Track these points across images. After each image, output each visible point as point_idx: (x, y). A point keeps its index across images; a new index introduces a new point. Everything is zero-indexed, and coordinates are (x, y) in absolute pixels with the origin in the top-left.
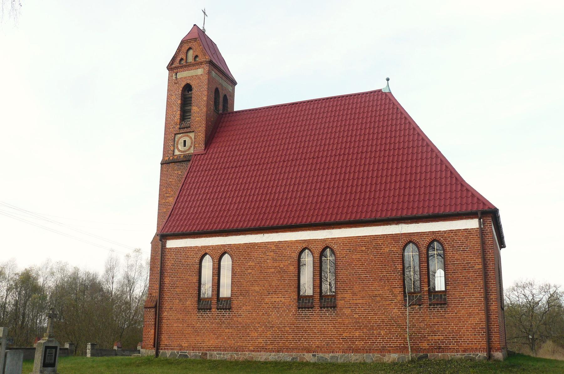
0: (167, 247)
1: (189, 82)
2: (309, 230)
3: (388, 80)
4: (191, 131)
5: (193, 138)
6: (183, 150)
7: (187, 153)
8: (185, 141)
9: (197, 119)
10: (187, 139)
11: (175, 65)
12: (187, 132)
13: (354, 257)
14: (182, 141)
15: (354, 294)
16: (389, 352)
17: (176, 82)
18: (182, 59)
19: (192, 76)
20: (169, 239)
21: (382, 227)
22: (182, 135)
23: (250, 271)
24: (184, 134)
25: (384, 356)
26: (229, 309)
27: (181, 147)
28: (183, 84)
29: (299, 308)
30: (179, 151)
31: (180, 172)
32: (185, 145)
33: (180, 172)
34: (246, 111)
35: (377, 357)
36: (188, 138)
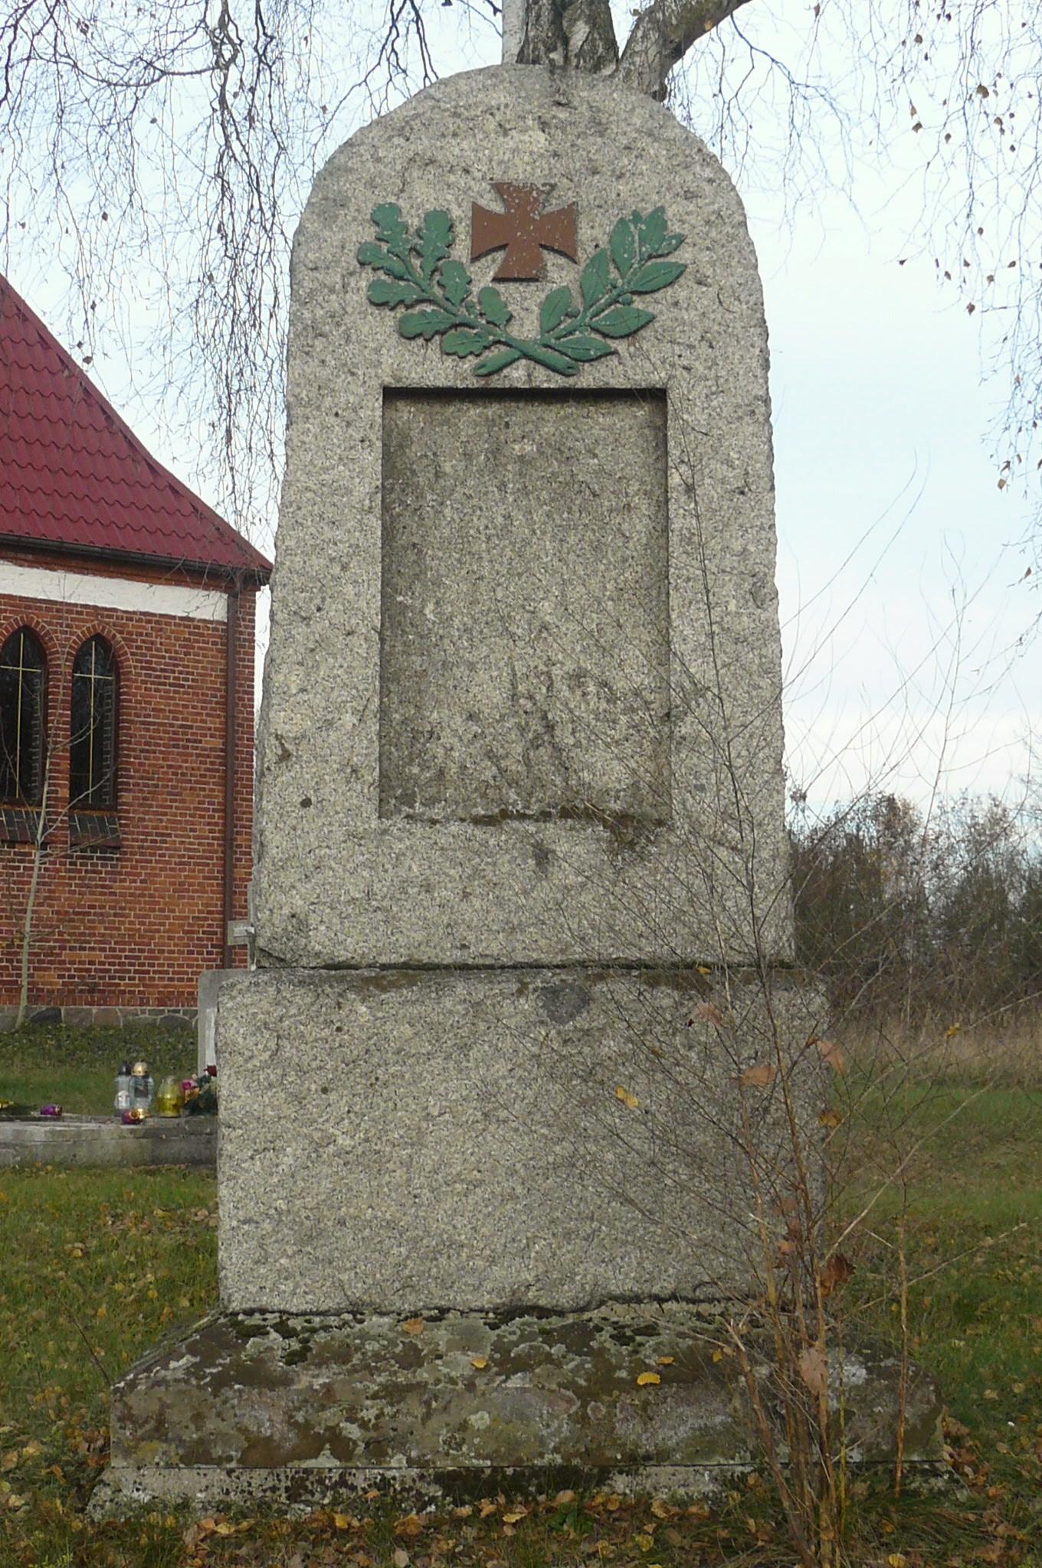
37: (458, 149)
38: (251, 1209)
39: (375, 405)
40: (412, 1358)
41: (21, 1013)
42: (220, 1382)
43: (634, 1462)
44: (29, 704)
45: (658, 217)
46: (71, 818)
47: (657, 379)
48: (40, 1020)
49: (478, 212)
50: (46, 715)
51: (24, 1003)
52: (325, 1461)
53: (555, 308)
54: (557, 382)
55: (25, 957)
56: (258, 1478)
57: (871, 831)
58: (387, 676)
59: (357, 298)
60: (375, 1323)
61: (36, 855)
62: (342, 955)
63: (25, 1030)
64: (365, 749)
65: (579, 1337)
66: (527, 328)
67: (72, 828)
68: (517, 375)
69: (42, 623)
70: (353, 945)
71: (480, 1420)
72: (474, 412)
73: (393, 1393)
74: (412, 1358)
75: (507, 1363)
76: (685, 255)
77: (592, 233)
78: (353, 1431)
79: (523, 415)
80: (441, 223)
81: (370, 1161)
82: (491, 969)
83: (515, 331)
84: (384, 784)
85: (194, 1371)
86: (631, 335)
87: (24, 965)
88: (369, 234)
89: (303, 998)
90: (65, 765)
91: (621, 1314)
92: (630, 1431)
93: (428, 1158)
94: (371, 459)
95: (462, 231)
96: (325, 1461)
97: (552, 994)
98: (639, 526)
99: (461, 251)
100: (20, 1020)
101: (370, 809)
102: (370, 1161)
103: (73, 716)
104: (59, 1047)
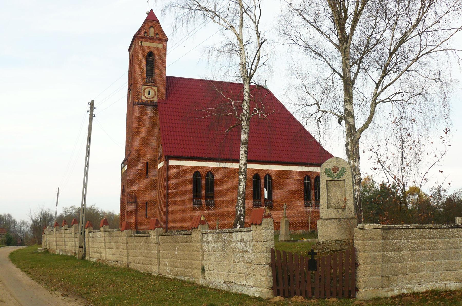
0: (170, 164)
1: (152, 50)
2: (259, 164)
3: (266, 81)
4: (155, 85)
5: (156, 90)
6: (148, 97)
7: (151, 100)
8: (149, 92)
9: (159, 78)
10: (151, 91)
11: (141, 35)
12: (151, 86)
13: (281, 181)
14: (147, 90)
15: (281, 200)
16: (298, 229)
17: (142, 48)
18: (146, 32)
19: (155, 48)
20: (171, 160)
21: (294, 167)
22: (147, 86)
23: (225, 184)
24: (149, 86)
25: (296, 231)
26: (213, 205)
27: (146, 94)
28: (148, 51)
29: (254, 206)
30: (146, 97)
31: (148, 112)
32: (149, 94)
33: (148, 112)
34: (181, 78)
35: (293, 232)
36: (152, 90)
37: (331, 164)
38: (320, 235)
39: (326, 181)
40: (330, 243)
41: (309, 231)
42: (318, 245)
43: (344, 250)
44: (308, 187)
45: (344, 167)
46: (315, 203)
47: (344, 179)
48: (312, 232)
49: (332, 168)
50: (311, 188)
51: (310, 229)
52: (324, 250)
53: (337, 174)
54: (338, 179)
55: (309, 223)
56: (320, 251)
57: (452, 198)
58: (327, 200)
59: (324, 175)
60: (328, 242)
61: (310, 208)
62: (325, 218)
63: (310, 233)
64: (326, 205)
65: (341, 242)
66: (336, 176)
67: (316, 204)
68: (335, 179)
69: (309, 174)
70: (326, 218)
71: (334, 247)
72: (333, 182)
73: (329, 245)
74: (330, 243)
75: (336, 244)
76: (346, 170)
77: (340, 169)
78: (326, 248)
79: (336, 182)
80: (330, 169)
81: (327, 231)
82: (335, 219)
83: (335, 176)
84: (328, 207)
85: (316, 245)
86: (342, 176)
87: (309, 224)
88: (325, 170)
89: (323, 221)
90: (314, 195)
91: (344, 241)
92: (343, 248)
93: (331, 231)
94: (326, 185)
95: (331, 169)
96: (324, 250)
97: (338, 220)
98: (344, 189)
99: (331, 171)
100: (309, 232)
101: (327, 209)
102: (327, 231)
103: (315, 188)
104: (315, 235)
